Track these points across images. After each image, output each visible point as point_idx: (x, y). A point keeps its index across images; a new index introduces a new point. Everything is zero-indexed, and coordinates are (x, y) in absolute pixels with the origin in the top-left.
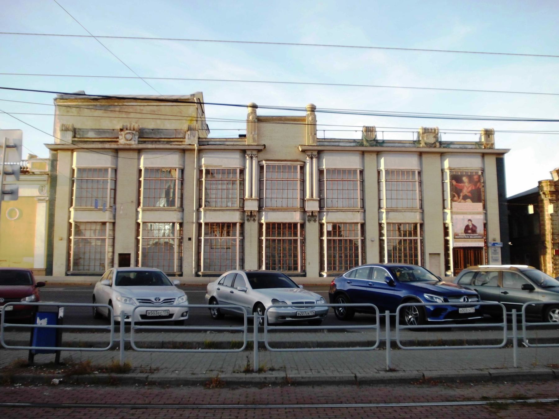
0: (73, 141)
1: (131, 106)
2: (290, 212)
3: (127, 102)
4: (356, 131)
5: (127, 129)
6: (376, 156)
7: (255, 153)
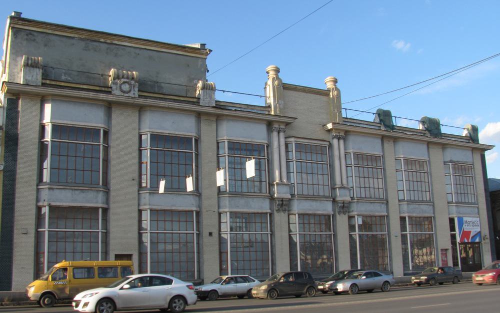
0: (42, 83)
1: (122, 47)
2: (322, 201)
3: (118, 40)
4: (224, 91)
5: (123, 77)
6: (393, 144)
7: (283, 127)
